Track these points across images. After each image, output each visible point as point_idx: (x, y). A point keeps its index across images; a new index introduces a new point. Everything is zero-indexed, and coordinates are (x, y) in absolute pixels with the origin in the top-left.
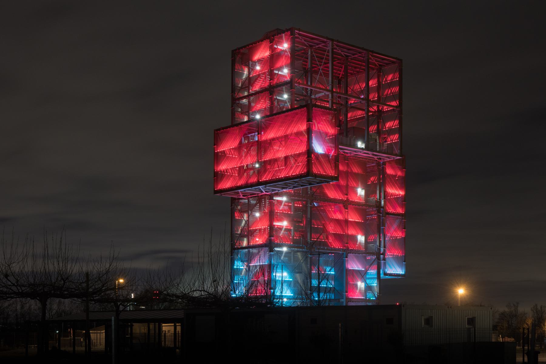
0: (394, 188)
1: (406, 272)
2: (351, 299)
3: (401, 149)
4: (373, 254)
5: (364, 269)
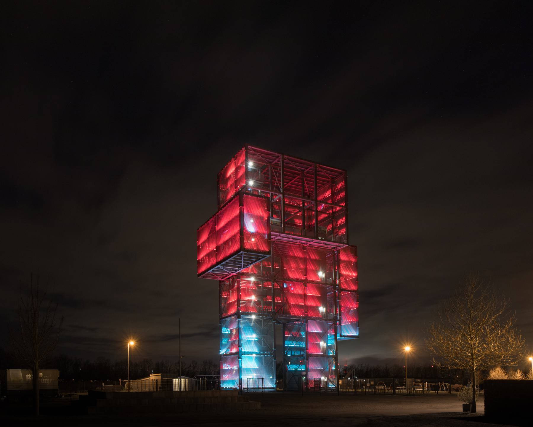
0: (348, 271)
1: (5, 375)
2: (311, 354)
3: (348, 239)
4: (330, 320)
5: (322, 332)
